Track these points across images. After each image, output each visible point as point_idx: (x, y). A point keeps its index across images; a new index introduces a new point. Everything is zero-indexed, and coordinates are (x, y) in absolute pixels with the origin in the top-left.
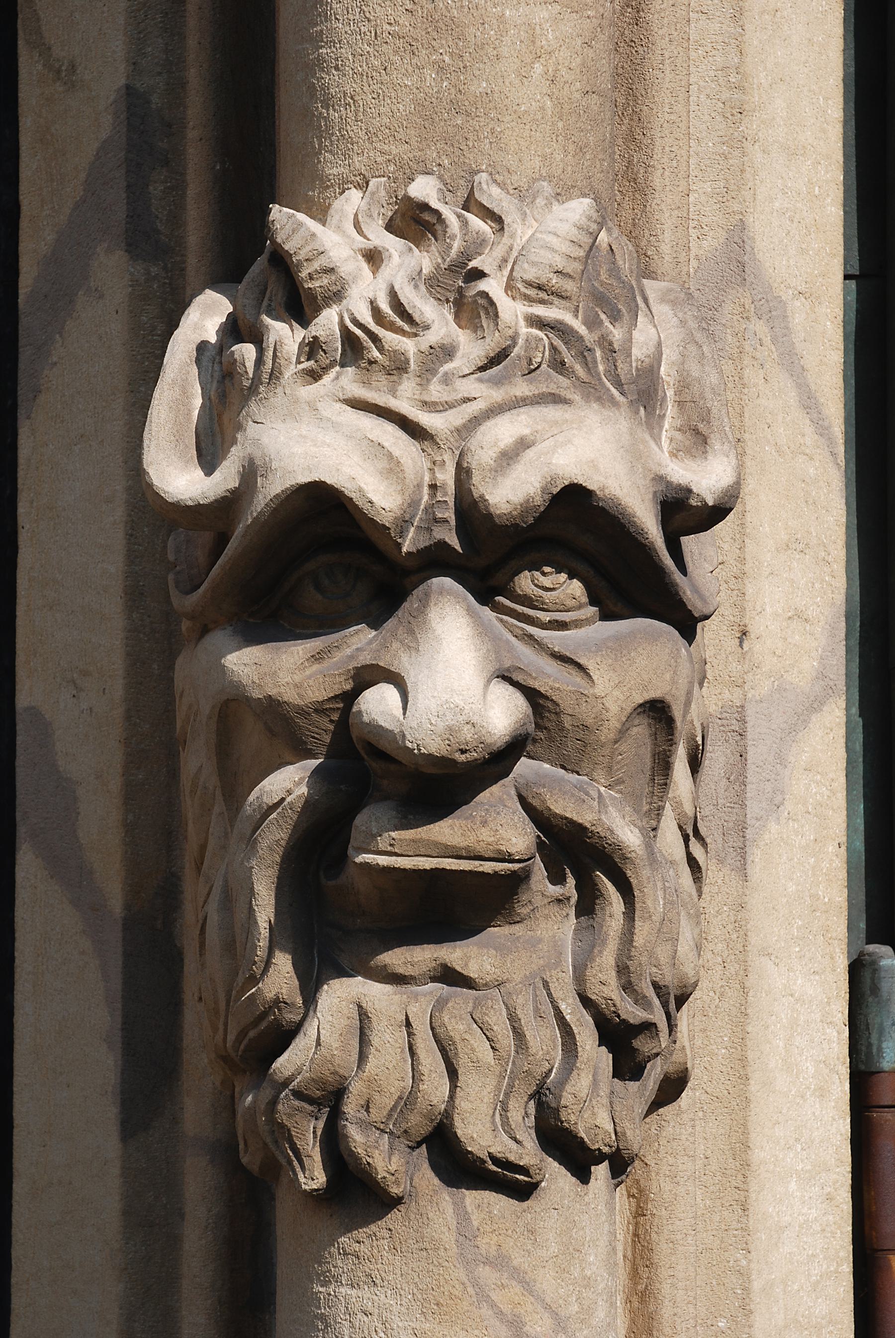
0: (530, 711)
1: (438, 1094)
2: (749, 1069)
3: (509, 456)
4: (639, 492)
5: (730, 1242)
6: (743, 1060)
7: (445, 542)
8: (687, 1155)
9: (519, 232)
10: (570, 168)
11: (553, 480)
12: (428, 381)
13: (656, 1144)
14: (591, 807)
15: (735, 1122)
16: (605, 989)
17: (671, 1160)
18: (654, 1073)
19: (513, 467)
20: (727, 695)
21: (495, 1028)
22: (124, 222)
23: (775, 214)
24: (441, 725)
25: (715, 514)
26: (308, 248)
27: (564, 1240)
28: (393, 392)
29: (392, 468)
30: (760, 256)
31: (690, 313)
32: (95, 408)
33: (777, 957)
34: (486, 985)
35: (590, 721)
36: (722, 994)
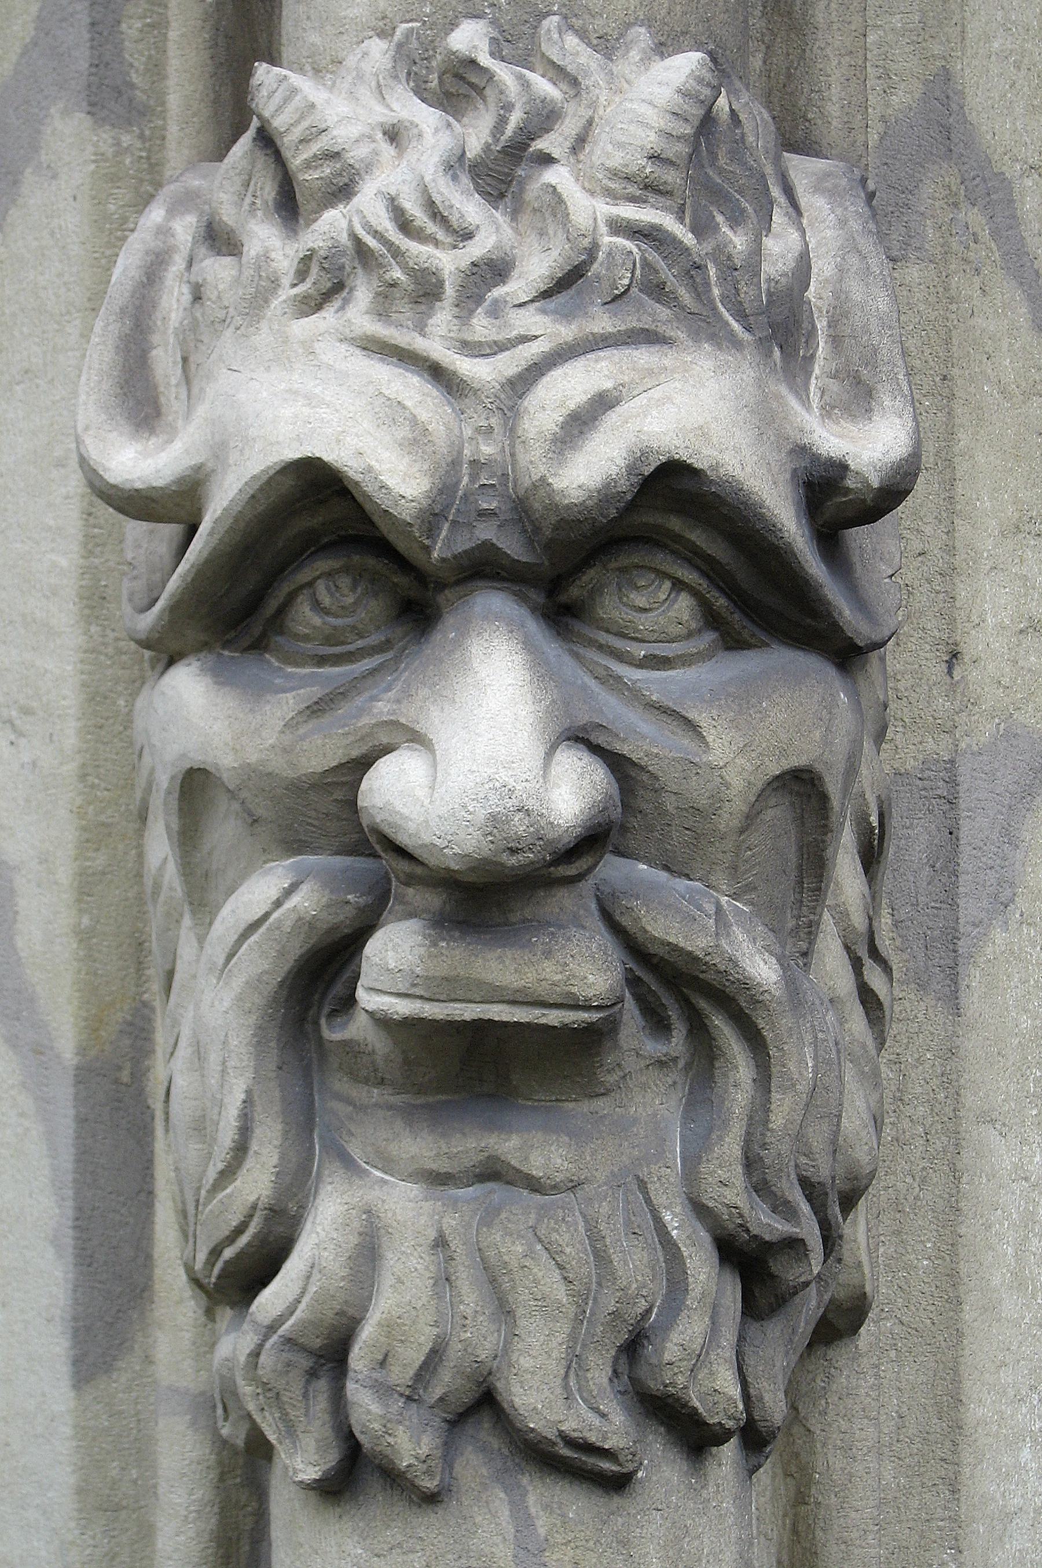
0: (614, 789)
1: (488, 1346)
2: (962, 1289)
3: (581, 422)
4: (769, 470)
5: (933, 1538)
6: (953, 1276)
7: (493, 544)
8: (866, 1417)
9: (602, 99)
10: (678, 7)
11: (645, 454)
12: (472, 312)
13: (823, 1402)
14: (704, 927)
15: (941, 1366)
16: (727, 1192)
17: (844, 1425)
18: (809, 1308)
19: (588, 436)
20: (930, 744)
21: (568, 1250)
22: (86, 73)
23: (993, 58)
24: (482, 814)
25: (890, 495)
26: (305, 124)
27: (671, 1554)
28: (421, 328)
29: (417, 439)
30: (972, 117)
31: (852, 208)
32: (44, 332)
33: (1004, 1124)
34: (554, 1187)
35: (703, 802)
36: (924, 1180)
